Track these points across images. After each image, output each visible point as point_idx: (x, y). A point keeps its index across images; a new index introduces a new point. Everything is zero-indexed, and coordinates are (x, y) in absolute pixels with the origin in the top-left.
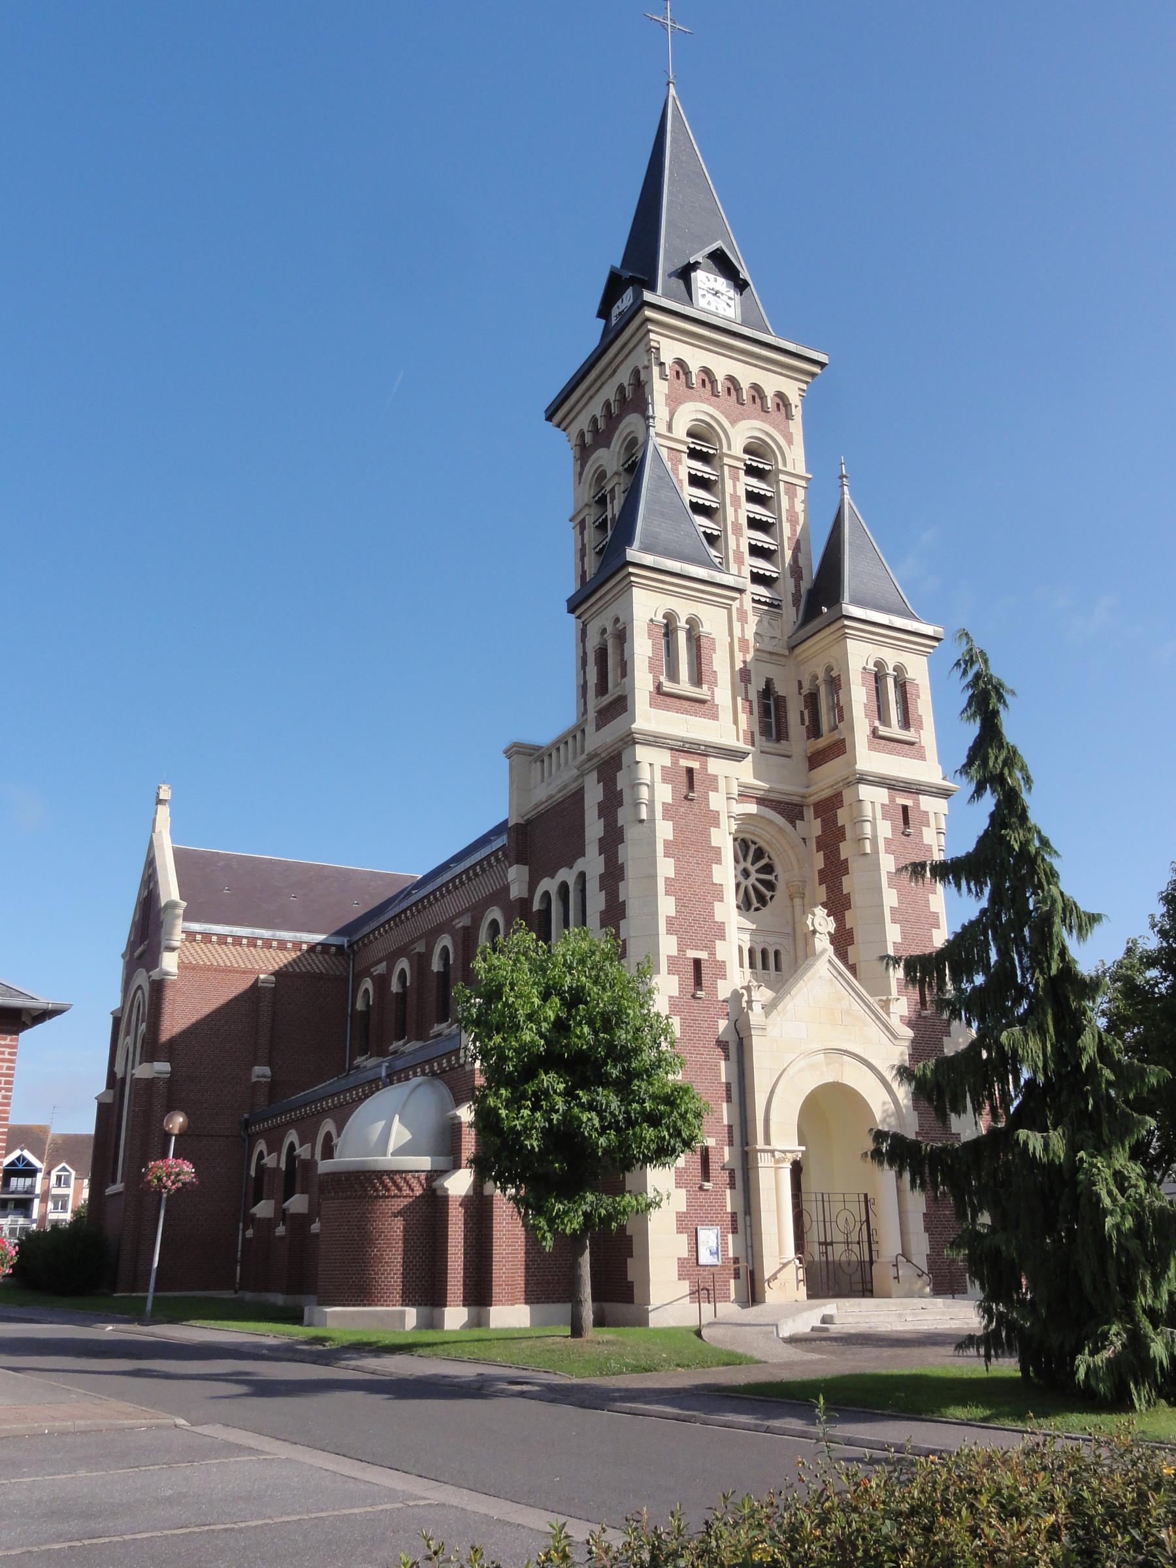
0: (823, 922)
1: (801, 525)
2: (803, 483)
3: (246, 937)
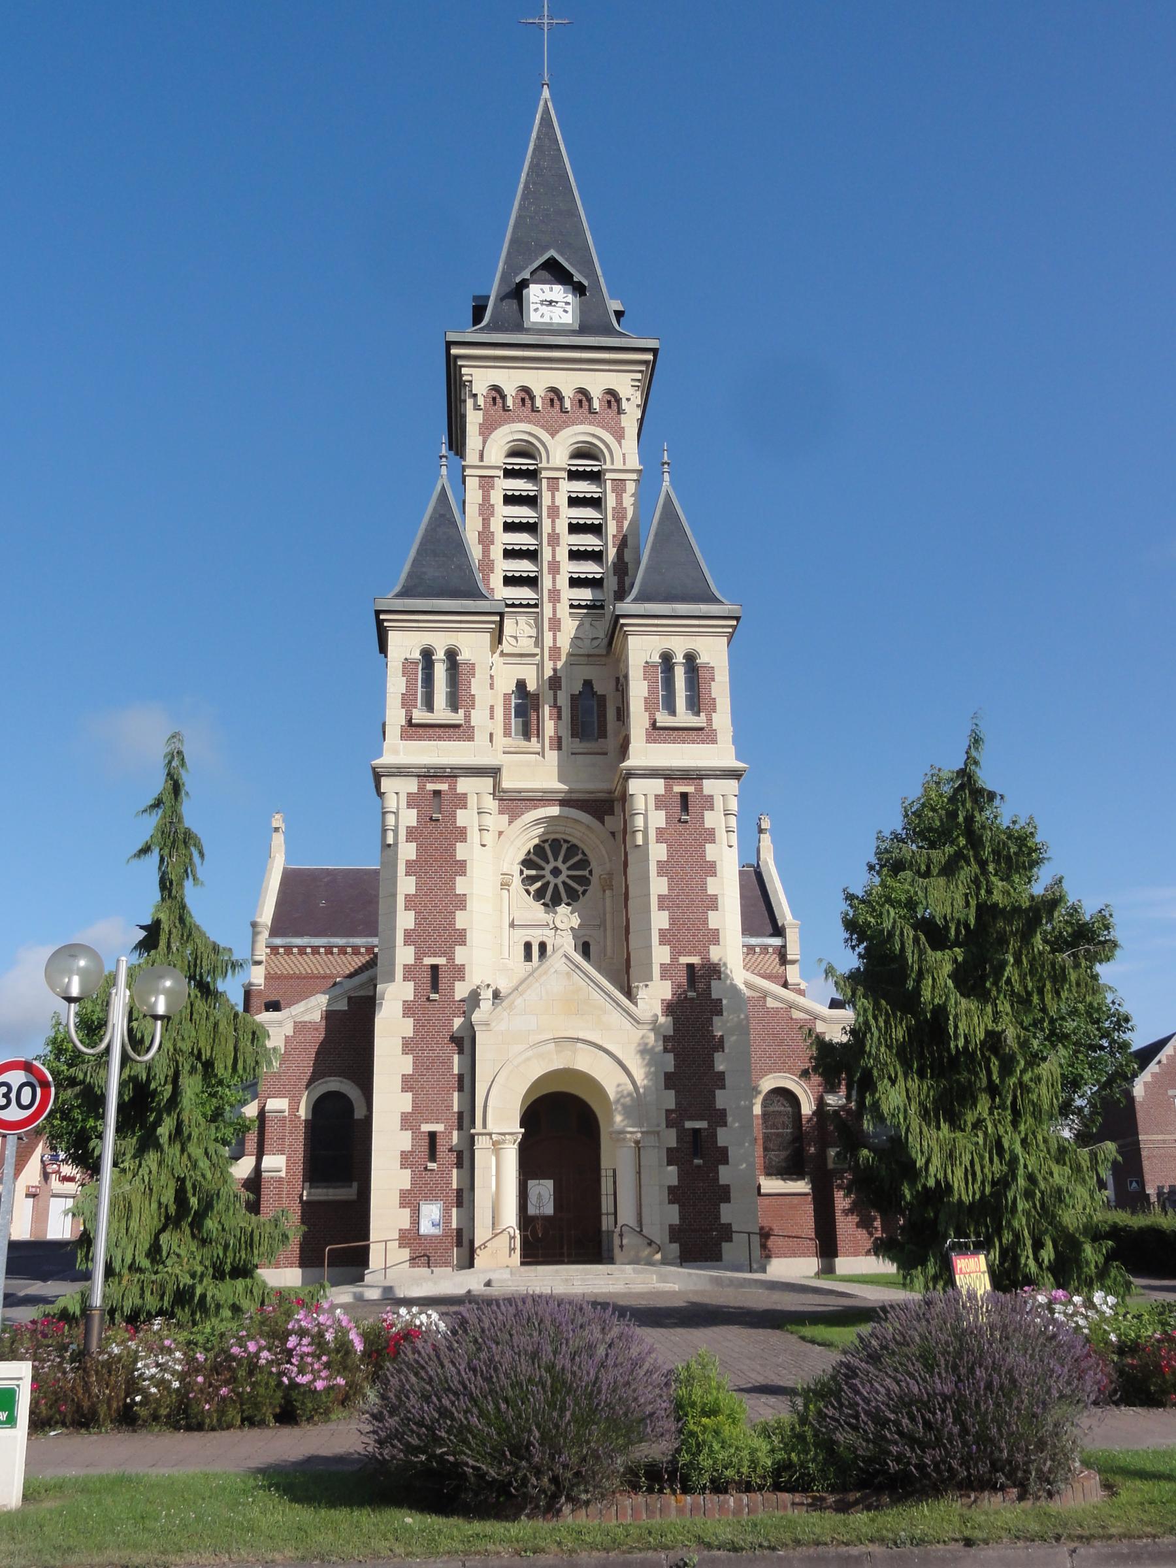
0: (565, 920)
1: (629, 519)
2: (634, 476)
3: (323, 947)
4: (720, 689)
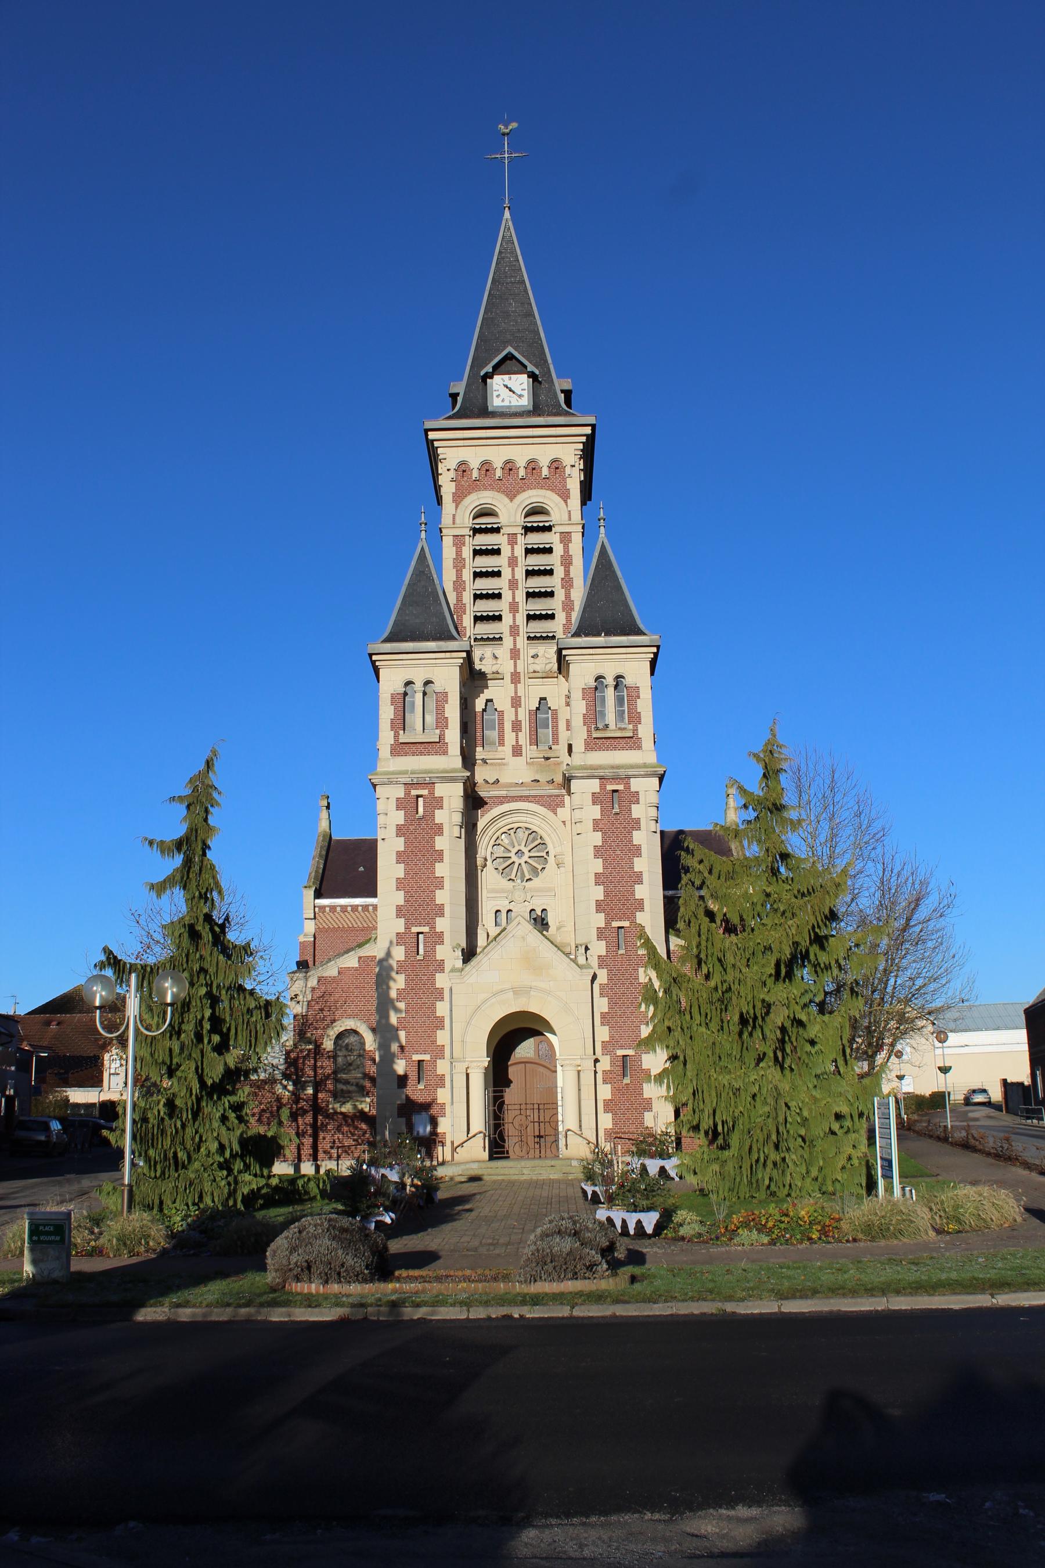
4: (645, 705)
